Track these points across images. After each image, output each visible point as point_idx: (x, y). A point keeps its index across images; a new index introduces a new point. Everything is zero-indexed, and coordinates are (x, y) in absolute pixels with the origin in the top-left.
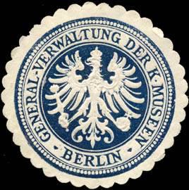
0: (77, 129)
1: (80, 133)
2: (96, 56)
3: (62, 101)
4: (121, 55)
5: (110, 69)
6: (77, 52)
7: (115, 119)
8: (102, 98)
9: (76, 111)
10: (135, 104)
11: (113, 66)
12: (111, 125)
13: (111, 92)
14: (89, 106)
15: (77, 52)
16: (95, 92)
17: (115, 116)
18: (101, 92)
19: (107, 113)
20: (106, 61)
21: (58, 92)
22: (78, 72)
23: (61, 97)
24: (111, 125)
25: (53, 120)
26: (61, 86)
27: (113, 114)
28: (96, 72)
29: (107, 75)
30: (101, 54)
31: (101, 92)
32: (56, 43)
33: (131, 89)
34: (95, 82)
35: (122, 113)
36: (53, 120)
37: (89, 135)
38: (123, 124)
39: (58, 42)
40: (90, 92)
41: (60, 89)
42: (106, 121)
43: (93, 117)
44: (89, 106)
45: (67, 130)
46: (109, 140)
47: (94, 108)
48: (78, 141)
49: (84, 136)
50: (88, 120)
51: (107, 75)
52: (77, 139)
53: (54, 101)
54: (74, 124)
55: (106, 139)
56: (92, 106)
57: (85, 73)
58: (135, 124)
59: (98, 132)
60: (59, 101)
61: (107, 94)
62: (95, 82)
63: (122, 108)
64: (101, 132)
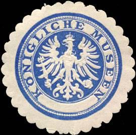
0: (56, 90)
1: (58, 92)
2: (69, 40)
3: (46, 69)
4: (88, 38)
5: (80, 47)
6: (56, 37)
7: (82, 81)
8: (74, 68)
9: (55, 77)
10: (95, 69)
11: (81, 45)
12: (81, 86)
13: (81, 65)
14: (64, 74)
15: (56, 37)
16: (69, 65)
17: (82, 78)
18: (74, 63)
19: (76, 76)
20: (76, 43)
21: (43, 62)
22: (57, 49)
23: (46, 66)
24: (81, 86)
25: (41, 82)
26: (47, 58)
27: (81, 78)
28: (70, 51)
29: (77, 52)
30: (59, 47)
31: (71, 83)
32: (97, 38)
33: (92, 59)
34: (69, 58)
35: (87, 77)
36: (41, 82)
37: (65, 94)
38: (88, 84)
39: (96, 36)
40: (65, 66)
41: (45, 61)
42: (77, 85)
43: (68, 82)
44: (64, 74)
45: (51, 89)
46: (81, 96)
47: (68, 74)
48: (56, 97)
49: (60, 94)
50: (65, 84)
51: (77, 52)
52: (55, 95)
53: (41, 68)
54: (54, 86)
55: (79, 96)
56: (66, 73)
57: (62, 50)
58: (96, 84)
59: (71, 91)
60: (44, 69)
61: (78, 66)
62: (69, 58)
63: (88, 74)
64: (72, 92)
